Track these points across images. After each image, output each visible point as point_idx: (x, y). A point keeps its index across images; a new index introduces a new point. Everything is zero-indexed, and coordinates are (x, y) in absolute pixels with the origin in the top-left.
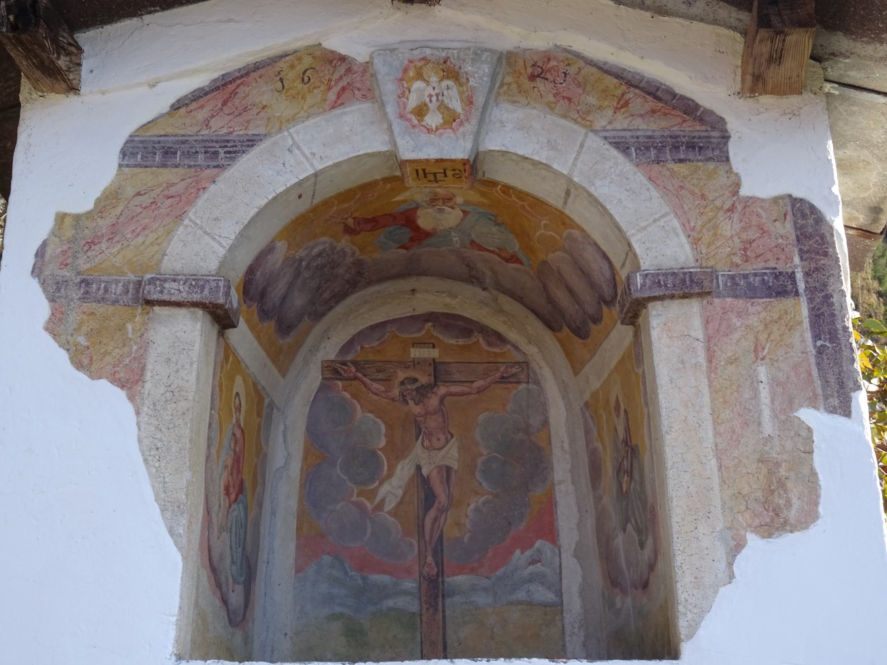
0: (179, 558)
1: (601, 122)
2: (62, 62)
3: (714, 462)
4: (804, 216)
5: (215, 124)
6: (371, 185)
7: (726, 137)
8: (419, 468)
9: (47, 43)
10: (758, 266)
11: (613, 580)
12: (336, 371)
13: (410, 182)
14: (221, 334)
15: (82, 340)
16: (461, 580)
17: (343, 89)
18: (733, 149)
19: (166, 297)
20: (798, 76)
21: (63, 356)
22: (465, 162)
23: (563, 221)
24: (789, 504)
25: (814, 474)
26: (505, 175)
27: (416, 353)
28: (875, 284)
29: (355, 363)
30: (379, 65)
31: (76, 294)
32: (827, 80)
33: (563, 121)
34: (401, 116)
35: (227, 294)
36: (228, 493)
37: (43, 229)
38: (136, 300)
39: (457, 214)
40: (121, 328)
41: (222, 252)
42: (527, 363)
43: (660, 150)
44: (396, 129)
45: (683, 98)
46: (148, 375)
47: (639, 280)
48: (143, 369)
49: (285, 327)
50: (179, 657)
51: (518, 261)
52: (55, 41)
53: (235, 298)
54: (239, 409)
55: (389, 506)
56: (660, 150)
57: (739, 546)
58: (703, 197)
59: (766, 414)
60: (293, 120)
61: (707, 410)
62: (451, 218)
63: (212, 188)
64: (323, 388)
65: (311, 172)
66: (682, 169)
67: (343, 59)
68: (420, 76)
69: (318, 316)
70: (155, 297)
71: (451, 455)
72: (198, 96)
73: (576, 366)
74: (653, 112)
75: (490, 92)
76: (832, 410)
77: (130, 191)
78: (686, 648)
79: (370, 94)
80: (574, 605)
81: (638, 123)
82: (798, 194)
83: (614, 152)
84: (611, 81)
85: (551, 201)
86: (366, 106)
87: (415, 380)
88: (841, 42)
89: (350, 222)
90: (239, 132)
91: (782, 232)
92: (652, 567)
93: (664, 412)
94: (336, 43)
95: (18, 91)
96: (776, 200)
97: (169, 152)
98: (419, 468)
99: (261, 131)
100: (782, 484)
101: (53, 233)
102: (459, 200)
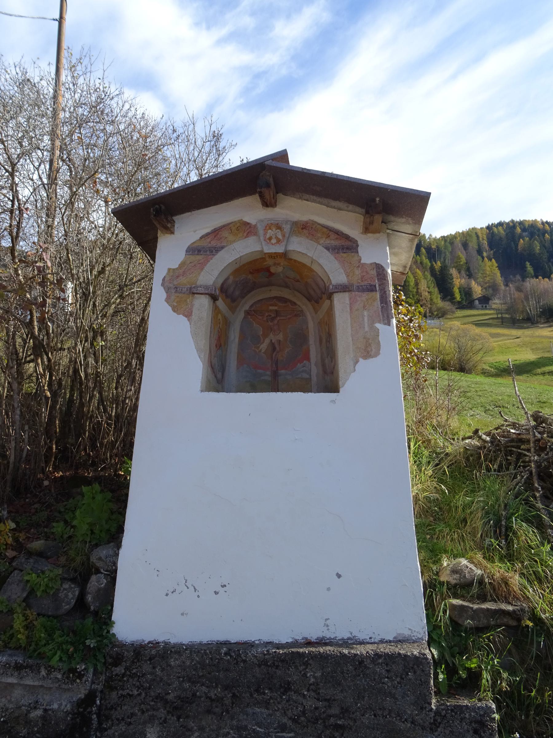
0: (201, 364)
1: (322, 241)
2: (169, 225)
3: (351, 339)
4: (379, 269)
5: (212, 243)
6: (257, 260)
7: (358, 246)
8: (271, 340)
9: (165, 220)
10: (366, 283)
11: (325, 372)
12: (248, 313)
13: (267, 259)
14: (214, 302)
15: (175, 304)
16: (283, 372)
17: (248, 232)
18: (359, 249)
19: (198, 292)
21: (170, 309)
22: (282, 253)
23: (310, 270)
24: (372, 350)
25: (379, 342)
26: (295, 257)
27: (271, 308)
28: (427, 289)
29: (254, 311)
30: (259, 226)
31: (173, 291)
32: (388, 229)
33: (311, 242)
34: (265, 240)
35: (215, 291)
36: (216, 347)
37: (164, 273)
38: (190, 293)
39: (282, 268)
40: (186, 301)
41: (214, 279)
42: (302, 311)
43: (338, 249)
44: (263, 244)
45: (346, 234)
46: (193, 314)
47: (331, 287)
48: (192, 312)
49: (233, 300)
50: (202, 391)
51: (299, 282)
52: (167, 219)
53: (218, 292)
54: (220, 323)
55: (263, 351)
56: (338, 249)
57: (357, 362)
58: (350, 263)
59: (366, 325)
60: (234, 241)
61: (349, 324)
62: (280, 269)
63: (211, 261)
64: (245, 318)
65: (239, 256)
66: (345, 255)
67: (248, 224)
68: (270, 229)
69: (243, 297)
70: (195, 292)
71: (280, 337)
72: (207, 235)
73: (316, 311)
74: (337, 238)
75: (290, 232)
76: (385, 324)
77: (188, 262)
78: (341, 390)
79: (256, 234)
80: (314, 379)
81: (333, 242)
82: (377, 262)
83: (325, 250)
84: (325, 230)
85: (308, 264)
86: (254, 237)
87: (270, 316)
88: (391, 218)
89: (251, 271)
90: (219, 245)
91: (373, 273)
92: (334, 368)
93: (337, 324)
94: (247, 219)
95: (157, 233)
96: (371, 264)
97: (199, 251)
98: (271, 340)
99: (225, 245)
100: (370, 345)
101: (167, 274)
102: (282, 264)
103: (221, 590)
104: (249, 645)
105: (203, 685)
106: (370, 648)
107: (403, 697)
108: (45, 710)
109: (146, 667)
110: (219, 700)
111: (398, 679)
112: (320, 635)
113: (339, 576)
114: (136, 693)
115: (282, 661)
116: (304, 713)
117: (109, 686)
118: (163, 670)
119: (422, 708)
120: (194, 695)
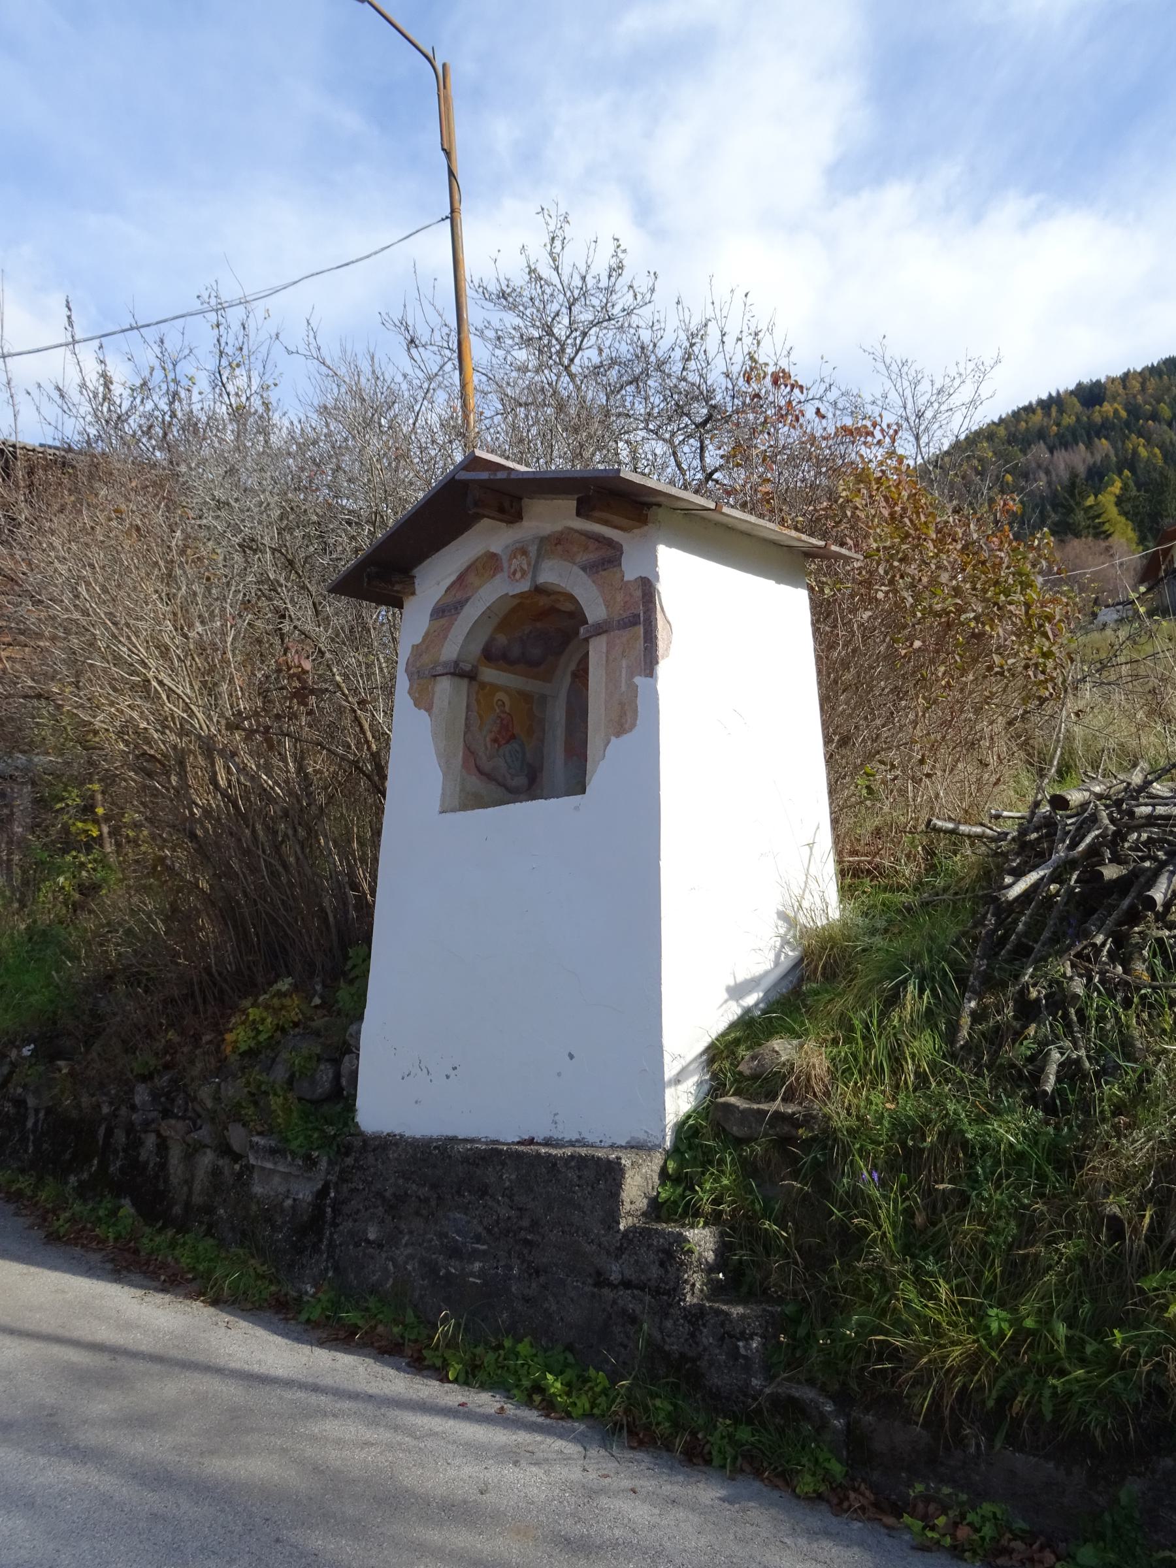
20: (241, 349)
68: (515, 557)
72: (453, 583)
76: (646, 676)
97: (443, 611)
103: (452, 1073)
104: (453, 1140)
105: (414, 1182)
106: (569, 1151)
107: (592, 1212)
108: (295, 1200)
109: (371, 1158)
110: (426, 1200)
111: (589, 1189)
112: (548, 1134)
113: (571, 1056)
114: (361, 1187)
115: (483, 1158)
116: (497, 1222)
117: (343, 1178)
118: (383, 1163)
119: (610, 1228)
120: (406, 1193)
